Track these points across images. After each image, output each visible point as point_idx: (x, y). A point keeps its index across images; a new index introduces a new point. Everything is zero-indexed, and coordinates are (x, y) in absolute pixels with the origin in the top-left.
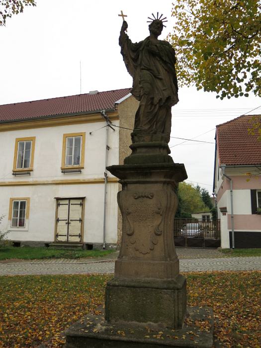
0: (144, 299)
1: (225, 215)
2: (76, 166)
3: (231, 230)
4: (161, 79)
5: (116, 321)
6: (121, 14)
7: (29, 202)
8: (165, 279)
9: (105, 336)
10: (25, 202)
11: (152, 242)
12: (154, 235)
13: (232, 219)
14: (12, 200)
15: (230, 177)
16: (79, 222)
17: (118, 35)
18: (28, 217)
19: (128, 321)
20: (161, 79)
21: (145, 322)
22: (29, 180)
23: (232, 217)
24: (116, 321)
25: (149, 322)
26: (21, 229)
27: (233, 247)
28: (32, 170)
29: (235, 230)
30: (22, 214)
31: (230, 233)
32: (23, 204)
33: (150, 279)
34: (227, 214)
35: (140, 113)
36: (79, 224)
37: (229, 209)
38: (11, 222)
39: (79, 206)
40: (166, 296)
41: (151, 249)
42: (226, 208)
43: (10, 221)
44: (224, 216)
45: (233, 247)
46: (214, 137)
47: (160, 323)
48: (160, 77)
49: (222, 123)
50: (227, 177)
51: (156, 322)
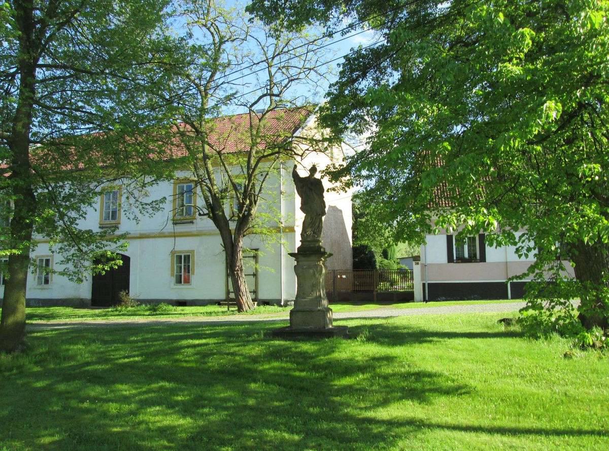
2: (113, 222)
3: (424, 282)
7: (194, 256)
9: (358, 387)
10: (189, 256)
14: (173, 253)
16: (252, 276)
18: (193, 273)
19: (262, 365)
22: (192, 230)
23: (424, 266)
26: (46, 286)
28: (120, 224)
29: (429, 282)
30: (188, 269)
31: (424, 285)
32: (187, 258)
36: (252, 279)
37: (422, 258)
38: (174, 279)
39: (252, 259)
43: (172, 277)
44: (417, 266)
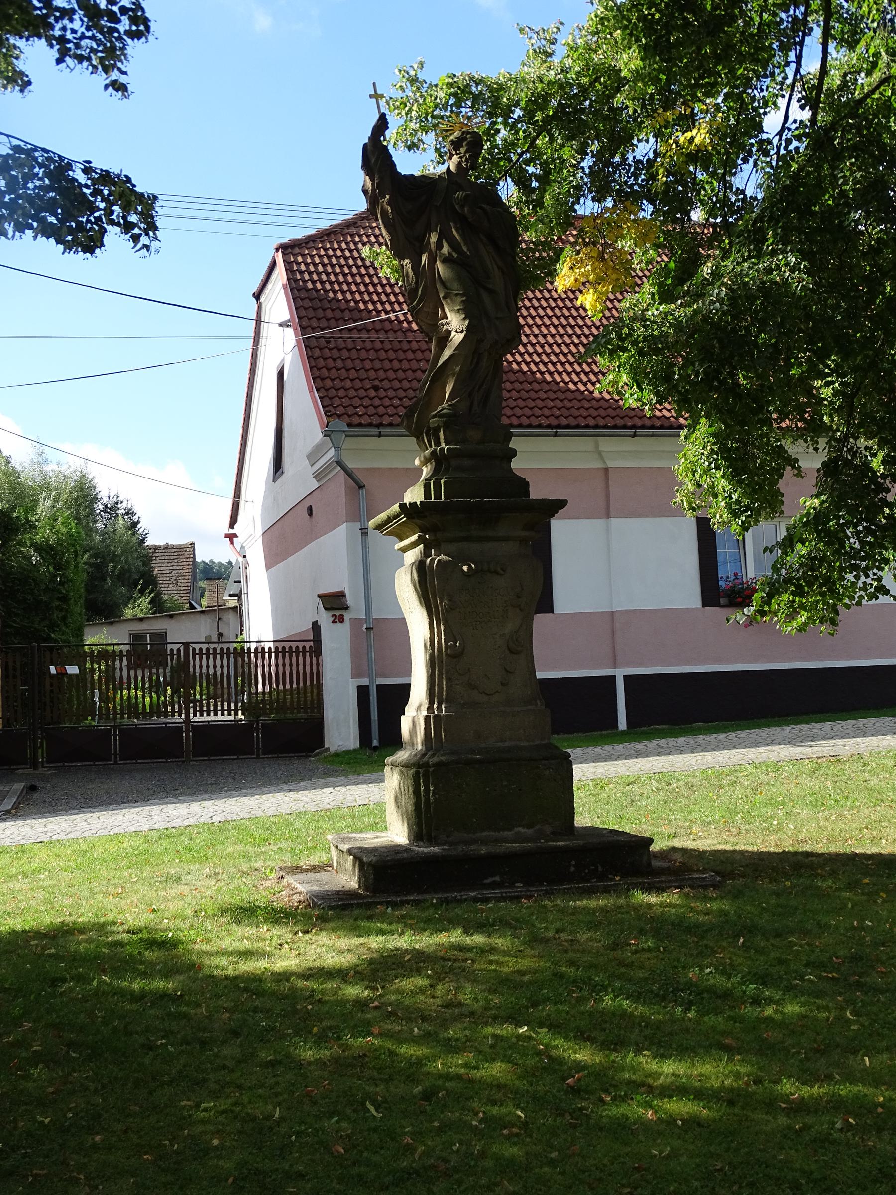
0: (505, 783)
1: (341, 620)
3: (365, 681)
4: (491, 292)
5: (448, 837)
6: (373, 93)
8: (537, 742)
11: (506, 670)
12: (507, 652)
13: (368, 638)
15: (361, 477)
17: (365, 137)
20: (491, 292)
21: (510, 830)
24: (448, 837)
25: (516, 829)
27: (375, 743)
31: (363, 692)
33: (507, 744)
34: (347, 617)
35: (609, 445)
40: (547, 773)
41: (502, 684)
42: (341, 595)
45: (375, 743)
46: (255, 288)
47: (537, 827)
48: (490, 286)
49: (299, 234)
50: (349, 473)
51: (529, 826)
